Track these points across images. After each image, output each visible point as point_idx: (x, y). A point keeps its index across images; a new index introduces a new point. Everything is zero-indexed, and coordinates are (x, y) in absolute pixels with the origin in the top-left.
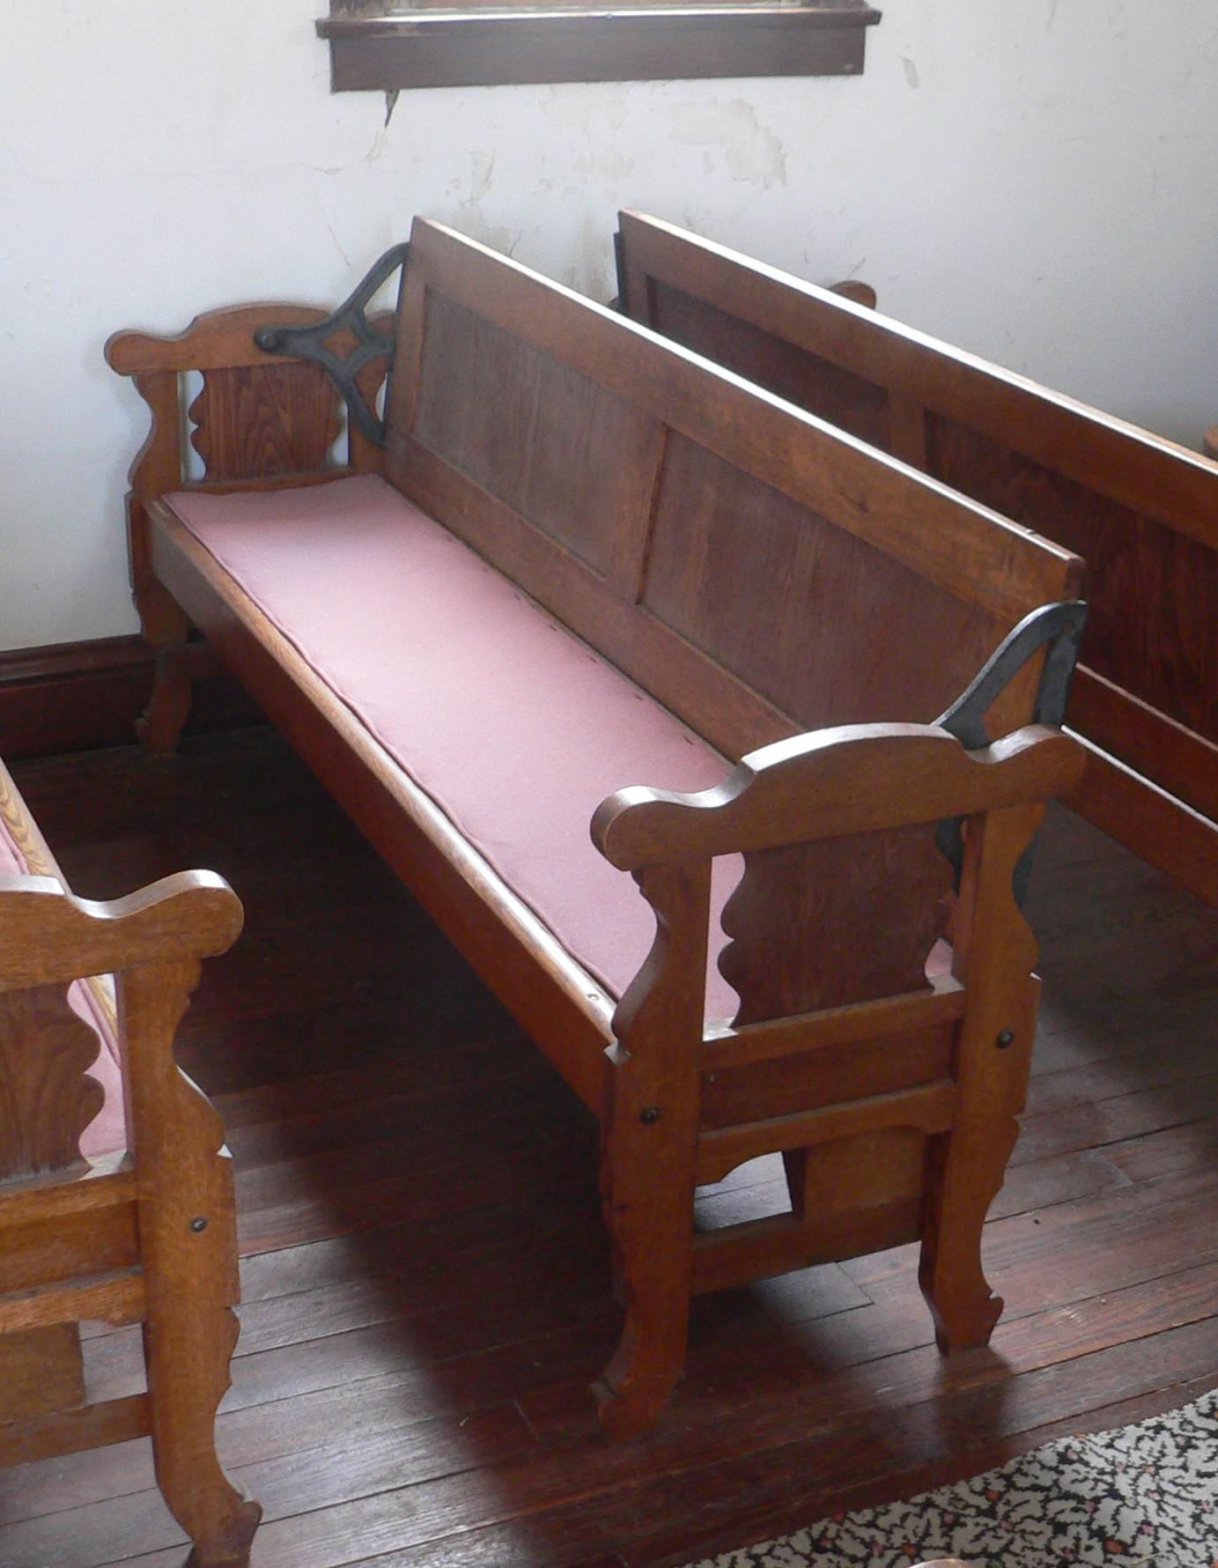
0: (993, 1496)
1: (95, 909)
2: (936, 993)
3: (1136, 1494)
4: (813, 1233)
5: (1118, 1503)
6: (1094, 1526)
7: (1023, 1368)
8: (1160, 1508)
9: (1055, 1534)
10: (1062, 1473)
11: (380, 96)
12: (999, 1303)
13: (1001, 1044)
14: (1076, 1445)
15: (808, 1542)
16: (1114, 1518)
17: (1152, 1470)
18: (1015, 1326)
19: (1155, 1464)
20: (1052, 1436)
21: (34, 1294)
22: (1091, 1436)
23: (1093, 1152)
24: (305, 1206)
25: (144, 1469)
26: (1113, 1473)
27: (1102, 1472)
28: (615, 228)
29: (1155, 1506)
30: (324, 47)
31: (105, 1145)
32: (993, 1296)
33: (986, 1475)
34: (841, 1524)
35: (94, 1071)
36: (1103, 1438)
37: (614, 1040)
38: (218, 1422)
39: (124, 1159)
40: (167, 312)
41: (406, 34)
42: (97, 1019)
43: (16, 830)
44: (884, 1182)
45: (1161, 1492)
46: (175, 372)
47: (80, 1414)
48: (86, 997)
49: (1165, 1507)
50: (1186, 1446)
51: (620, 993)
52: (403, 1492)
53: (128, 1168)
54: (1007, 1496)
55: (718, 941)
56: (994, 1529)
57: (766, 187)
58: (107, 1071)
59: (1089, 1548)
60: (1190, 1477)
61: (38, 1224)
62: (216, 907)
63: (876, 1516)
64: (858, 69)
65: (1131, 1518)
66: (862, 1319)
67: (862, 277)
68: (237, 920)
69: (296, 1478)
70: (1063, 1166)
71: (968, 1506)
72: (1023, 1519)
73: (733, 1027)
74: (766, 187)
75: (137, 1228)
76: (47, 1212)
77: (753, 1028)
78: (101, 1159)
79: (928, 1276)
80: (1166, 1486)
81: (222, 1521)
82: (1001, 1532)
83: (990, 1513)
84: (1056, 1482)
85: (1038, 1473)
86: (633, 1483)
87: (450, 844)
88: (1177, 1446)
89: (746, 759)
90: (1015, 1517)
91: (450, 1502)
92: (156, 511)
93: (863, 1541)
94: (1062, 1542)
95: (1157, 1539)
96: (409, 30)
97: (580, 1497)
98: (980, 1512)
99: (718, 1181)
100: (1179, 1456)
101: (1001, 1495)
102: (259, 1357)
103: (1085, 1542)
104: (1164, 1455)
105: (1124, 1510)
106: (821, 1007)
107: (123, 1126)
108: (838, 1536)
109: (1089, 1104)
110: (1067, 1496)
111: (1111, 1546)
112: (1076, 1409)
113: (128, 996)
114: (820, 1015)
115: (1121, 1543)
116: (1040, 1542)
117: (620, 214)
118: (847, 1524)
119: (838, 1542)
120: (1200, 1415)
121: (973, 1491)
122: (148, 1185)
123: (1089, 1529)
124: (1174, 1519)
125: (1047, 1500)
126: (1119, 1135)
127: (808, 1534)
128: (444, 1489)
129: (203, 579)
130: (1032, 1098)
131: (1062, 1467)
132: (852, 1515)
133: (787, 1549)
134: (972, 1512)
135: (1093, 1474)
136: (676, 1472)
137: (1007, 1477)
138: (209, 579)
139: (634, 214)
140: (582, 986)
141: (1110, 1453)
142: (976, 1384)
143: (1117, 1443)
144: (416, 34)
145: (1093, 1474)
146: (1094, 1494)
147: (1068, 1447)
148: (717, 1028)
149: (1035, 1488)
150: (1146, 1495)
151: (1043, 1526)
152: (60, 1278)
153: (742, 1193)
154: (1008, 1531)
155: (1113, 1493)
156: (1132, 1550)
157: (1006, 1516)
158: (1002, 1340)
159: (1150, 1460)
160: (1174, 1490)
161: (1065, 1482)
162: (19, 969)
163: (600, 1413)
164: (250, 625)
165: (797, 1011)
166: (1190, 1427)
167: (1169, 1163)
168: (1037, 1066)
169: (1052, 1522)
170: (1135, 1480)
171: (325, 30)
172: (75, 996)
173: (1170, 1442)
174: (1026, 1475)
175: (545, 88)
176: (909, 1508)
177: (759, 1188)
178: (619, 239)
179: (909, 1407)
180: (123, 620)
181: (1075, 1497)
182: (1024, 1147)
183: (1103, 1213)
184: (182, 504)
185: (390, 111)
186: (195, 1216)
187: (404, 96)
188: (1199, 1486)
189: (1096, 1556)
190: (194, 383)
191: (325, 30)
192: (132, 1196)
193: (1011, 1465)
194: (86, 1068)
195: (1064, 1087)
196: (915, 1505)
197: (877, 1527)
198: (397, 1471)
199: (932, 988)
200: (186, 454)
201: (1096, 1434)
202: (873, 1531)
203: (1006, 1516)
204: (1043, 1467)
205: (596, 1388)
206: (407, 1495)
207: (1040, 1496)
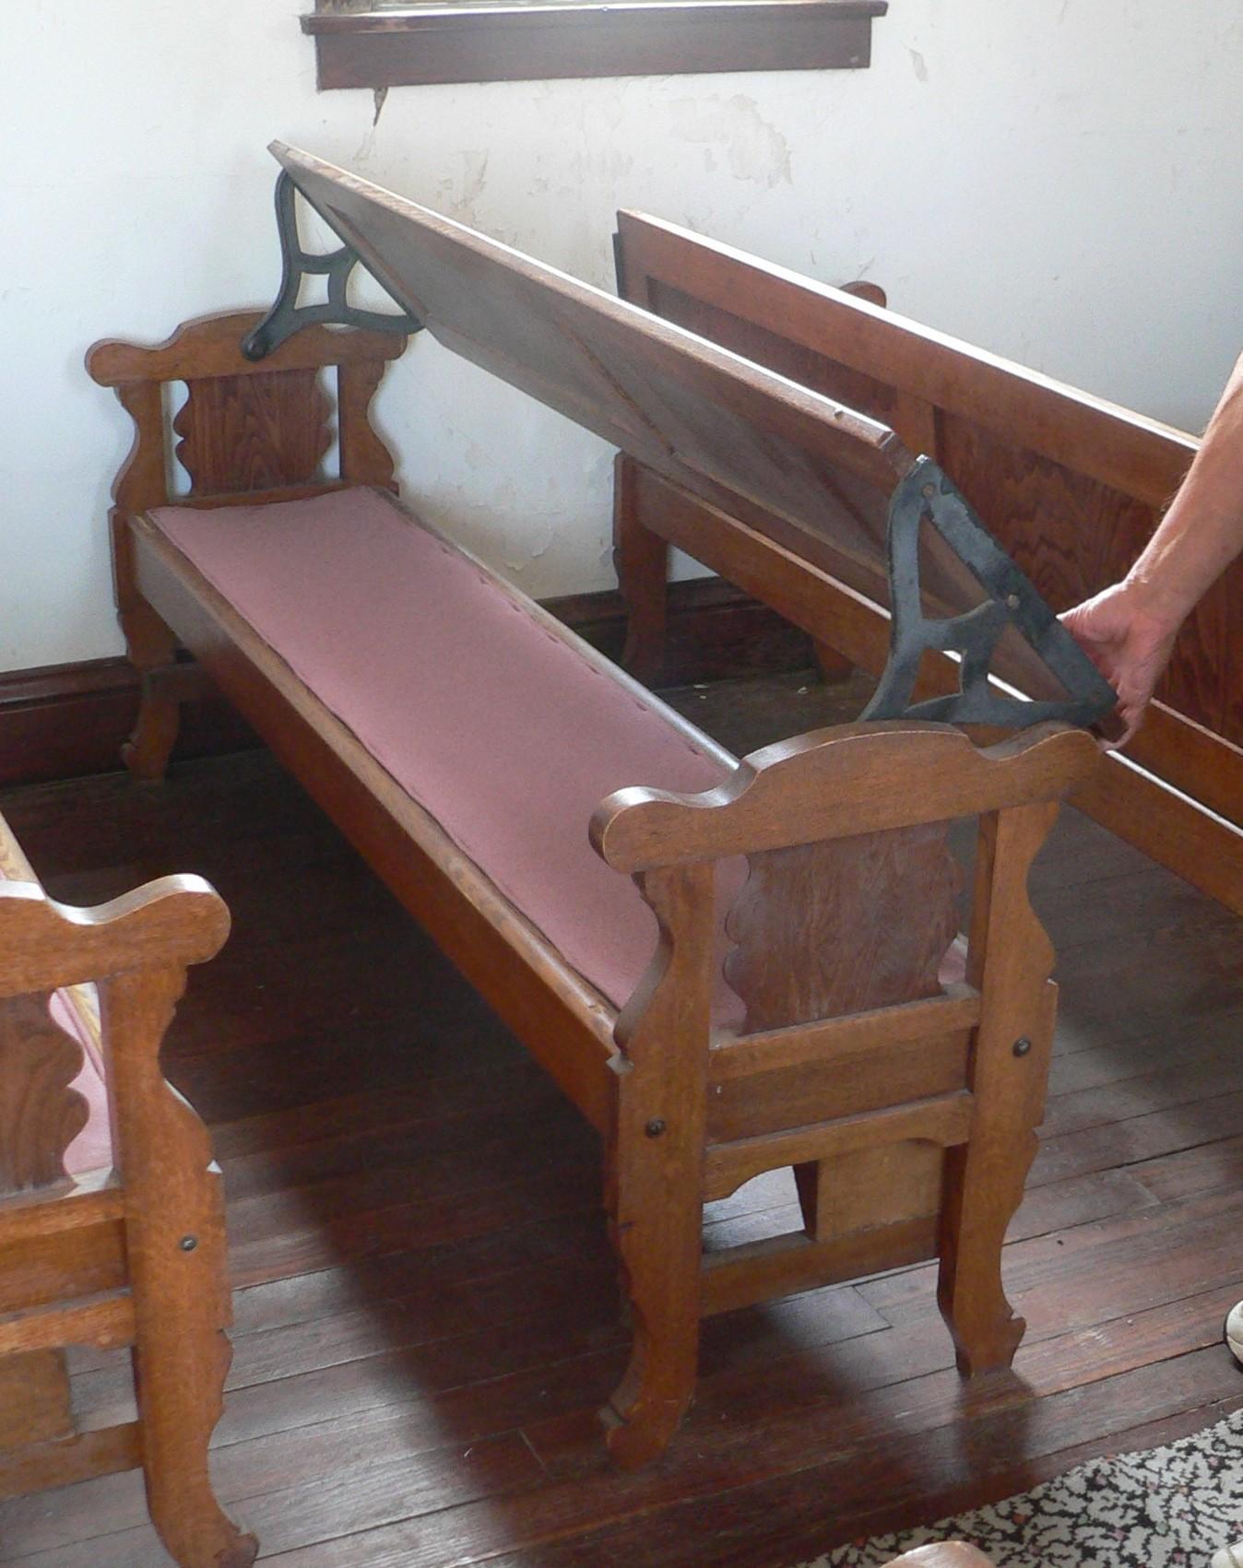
0: (1021, 1520)
1: (76, 915)
3: (1168, 1517)
4: (813, 1257)
5: (1149, 1531)
6: (1125, 1553)
8: (1194, 1530)
9: (1084, 1558)
10: (1090, 1500)
11: (367, 95)
12: (1021, 1324)
13: (1017, 1052)
14: (1106, 1468)
17: (1185, 1490)
18: (1038, 1348)
20: (1078, 1459)
21: (17, 1318)
22: (1122, 1456)
24: (300, 1236)
25: (137, 1505)
26: (1144, 1496)
27: (1132, 1496)
29: (1188, 1527)
30: (308, 45)
31: (89, 1162)
33: (1012, 1499)
34: (862, 1548)
35: (77, 1084)
36: (1134, 1458)
37: (616, 1051)
38: (211, 1457)
39: (111, 1175)
40: (152, 324)
41: (395, 30)
42: (76, 1026)
44: (905, 1196)
45: (1195, 1512)
46: (158, 383)
47: (69, 1444)
48: (68, 1010)
49: (1199, 1528)
50: (1220, 1467)
52: (405, 1525)
54: (1034, 1520)
56: (1020, 1553)
58: (91, 1084)
60: (1224, 1499)
61: (24, 1244)
62: (202, 912)
63: (898, 1541)
64: (865, 63)
65: (1162, 1547)
68: (223, 926)
69: (294, 1512)
71: (993, 1530)
72: (1051, 1543)
76: (30, 1231)
80: (1199, 1506)
82: (1028, 1557)
83: (1017, 1537)
84: (1085, 1510)
85: (1067, 1499)
88: (1210, 1467)
90: (1043, 1541)
91: (455, 1533)
92: (140, 525)
96: (397, 25)
97: (588, 1527)
98: (1006, 1536)
100: (1212, 1477)
101: (1028, 1519)
102: (255, 1390)
104: (1196, 1477)
105: (1154, 1539)
106: (833, 1013)
107: (108, 1144)
109: (1111, 1123)
110: (1097, 1524)
112: (1101, 1431)
113: (111, 1007)
114: (829, 1025)
117: (619, 214)
118: (869, 1549)
120: (1233, 1432)
121: (998, 1515)
122: (134, 1202)
124: (1208, 1540)
125: (1075, 1526)
127: (829, 1559)
128: (448, 1521)
131: (1090, 1494)
132: (874, 1540)
134: (998, 1536)
135: (1123, 1500)
136: (688, 1500)
139: (633, 214)
140: (582, 1001)
141: (1140, 1474)
143: (1148, 1464)
144: (405, 29)
145: (1123, 1500)
146: (1122, 1523)
147: (1097, 1471)
149: (1063, 1514)
150: (1179, 1516)
151: (1072, 1550)
152: (47, 1300)
153: (755, 1218)
154: (1035, 1555)
155: (1144, 1520)
157: (1034, 1540)
158: (1029, 1363)
159: (1183, 1481)
160: (1209, 1511)
161: (1094, 1510)
165: (806, 1018)
166: (1222, 1447)
167: (1196, 1177)
168: (1055, 1084)
169: (1080, 1546)
170: (1168, 1501)
171: (311, 26)
172: (57, 1007)
173: (1203, 1464)
174: (1054, 1501)
178: (618, 240)
179: (931, 1431)
180: (108, 642)
181: (1103, 1524)
182: (1041, 1168)
184: (168, 520)
187: (395, 95)
188: (1234, 1507)
190: (178, 394)
191: (311, 26)
192: (118, 1214)
193: (1038, 1491)
195: (1087, 1106)
198: (399, 1504)
201: (1127, 1454)
203: (1034, 1540)
204: (1072, 1494)
205: (605, 1415)
206: (409, 1527)
207: (1070, 1522)
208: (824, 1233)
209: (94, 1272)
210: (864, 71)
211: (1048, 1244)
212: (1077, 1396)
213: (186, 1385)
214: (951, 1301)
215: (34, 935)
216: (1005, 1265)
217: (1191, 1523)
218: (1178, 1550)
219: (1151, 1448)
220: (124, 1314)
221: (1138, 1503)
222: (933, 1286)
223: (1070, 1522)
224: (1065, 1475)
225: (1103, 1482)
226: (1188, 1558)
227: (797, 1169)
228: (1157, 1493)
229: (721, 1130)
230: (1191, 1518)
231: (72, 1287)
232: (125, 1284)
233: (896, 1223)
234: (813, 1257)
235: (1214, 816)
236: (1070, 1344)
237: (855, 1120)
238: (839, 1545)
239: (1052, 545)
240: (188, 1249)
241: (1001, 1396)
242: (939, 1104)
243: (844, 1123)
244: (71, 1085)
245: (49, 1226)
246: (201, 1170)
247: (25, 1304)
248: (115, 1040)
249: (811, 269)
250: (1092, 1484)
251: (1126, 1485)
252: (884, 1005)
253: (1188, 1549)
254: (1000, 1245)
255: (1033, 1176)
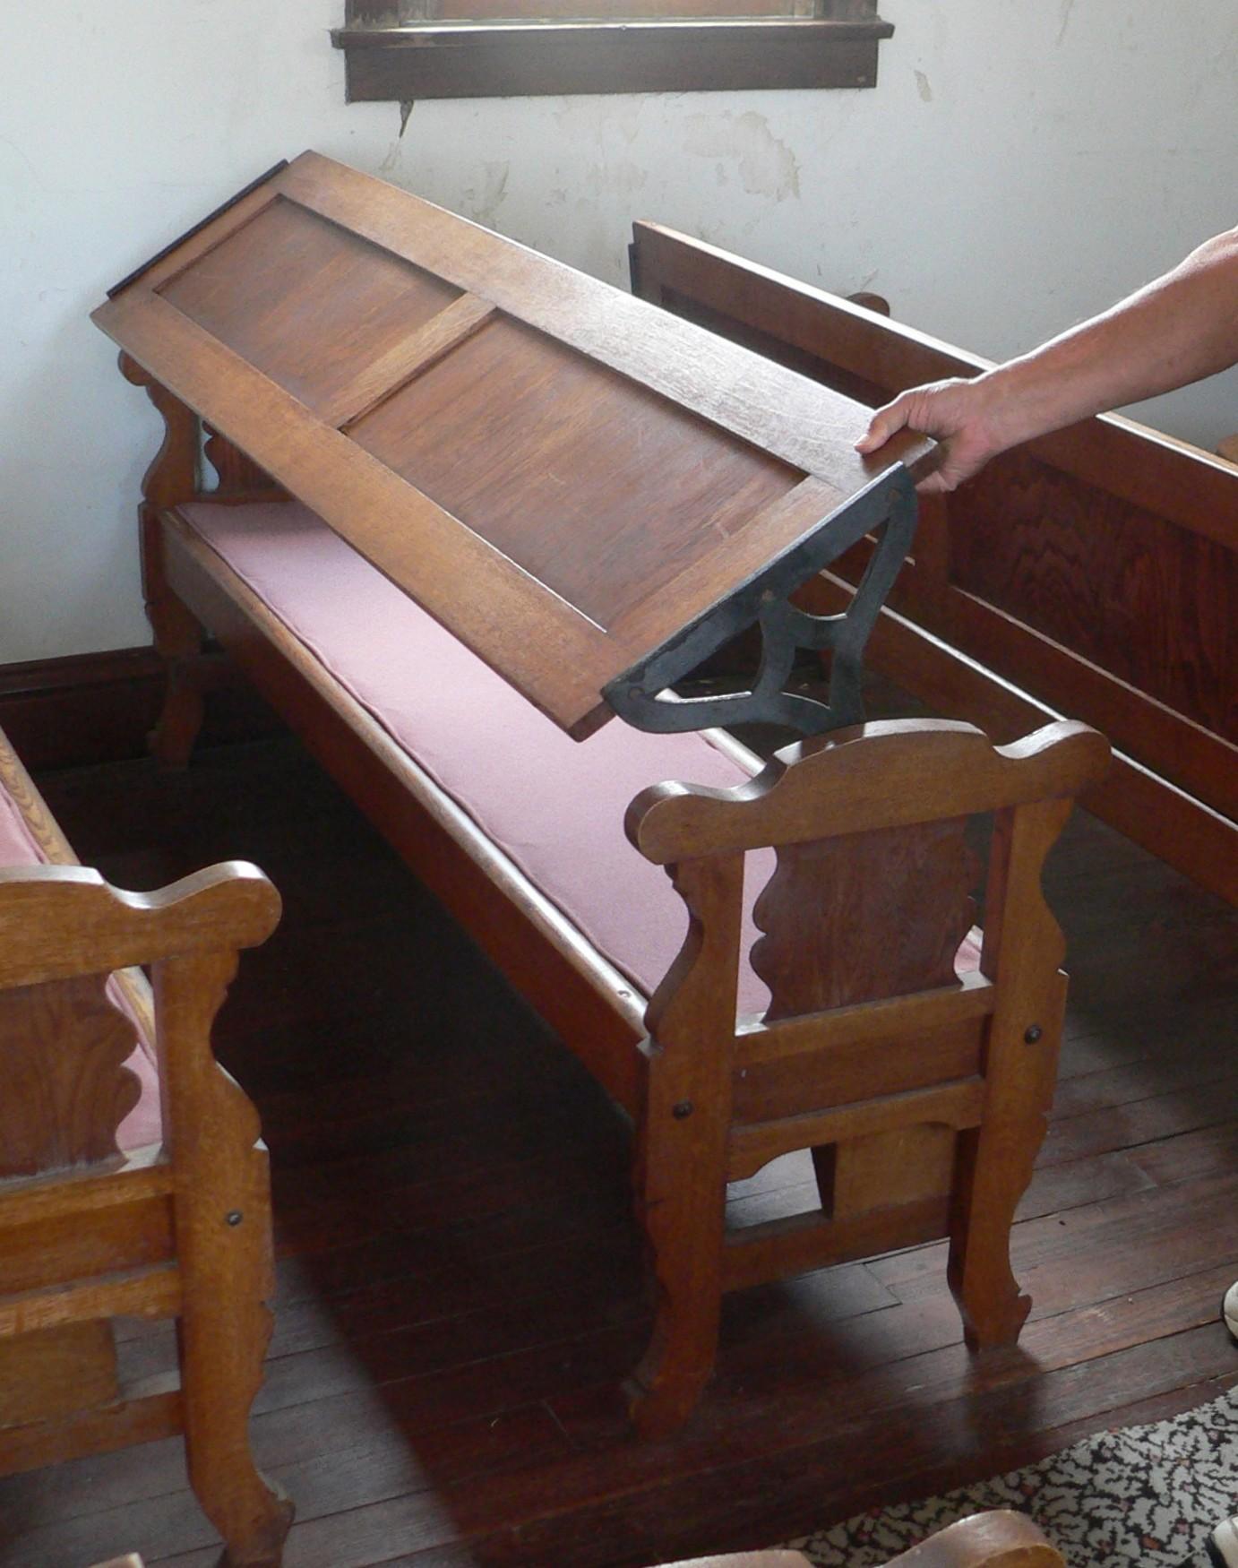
1: (134, 900)
2: (965, 988)
3: (1171, 1488)
4: (835, 1233)
5: (1153, 1502)
6: (1130, 1523)
7: (1051, 1366)
8: (1196, 1501)
11: (394, 108)
13: (1028, 1039)
14: (1110, 1441)
18: (1043, 1325)
19: (1189, 1458)
22: (1126, 1430)
23: (1116, 1155)
26: (1148, 1468)
27: (1136, 1468)
28: (630, 239)
30: (339, 57)
31: (140, 1140)
33: (1023, 1471)
34: (877, 1518)
35: (129, 1064)
36: (1137, 1432)
37: (647, 1035)
43: (40, 833)
44: (916, 1176)
45: (1197, 1484)
51: (652, 991)
53: (164, 1161)
55: (750, 934)
57: (779, 199)
58: (143, 1064)
59: (1125, 1542)
62: (254, 897)
63: (912, 1510)
64: (871, 82)
65: (1165, 1518)
66: (891, 1320)
68: (274, 913)
73: (764, 1022)
74: (779, 199)
76: (84, 1204)
77: (785, 1025)
78: (137, 1152)
79: (956, 1276)
80: (1201, 1479)
81: (255, 1521)
84: (1091, 1481)
87: (476, 846)
88: (1210, 1441)
89: (778, 753)
90: (1051, 1511)
92: (170, 521)
93: (899, 1534)
95: (1192, 1537)
99: (751, 1176)
100: (1213, 1450)
101: (1036, 1490)
103: (1121, 1535)
105: (1158, 1510)
106: (855, 1000)
108: (875, 1530)
110: (1103, 1495)
111: (1147, 1542)
112: (1105, 1406)
115: (1158, 1541)
116: (1076, 1536)
117: (635, 226)
118: (883, 1519)
119: (875, 1536)
123: (1124, 1525)
124: (1210, 1511)
125: (1081, 1497)
126: (1143, 1138)
127: (845, 1528)
129: (219, 588)
132: (889, 1509)
133: (824, 1544)
135: (1127, 1472)
136: (708, 1470)
138: (227, 589)
139: (649, 225)
141: (1144, 1447)
143: (1151, 1437)
144: (431, 44)
145: (1127, 1472)
146: (1127, 1494)
147: (1102, 1444)
148: (748, 1025)
149: (1071, 1485)
150: (1182, 1488)
152: (98, 1272)
155: (1148, 1492)
156: (1168, 1548)
157: (1042, 1510)
158: (1033, 1338)
159: (1185, 1455)
160: (1210, 1483)
161: (1099, 1481)
162: (58, 960)
163: (632, 1411)
164: (269, 634)
166: (1222, 1421)
167: (1195, 1164)
170: (1170, 1473)
173: (1203, 1438)
174: (1061, 1473)
175: (559, 99)
176: (945, 1503)
178: (634, 251)
180: (135, 631)
181: (1109, 1496)
182: (1050, 1148)
184: (197, 515)
185: (404, 123)
186: (230, 1210)
187: (420, 107)
189: (1133, 1549)
191: (341, 40)
192: (168, 1188)
193: (1046, 1463)
194: (125, 1057)
196: (951, 1500)
197: (913, 1521)
199: (961, 983)
200: (199, 464)
202: (909, 1525)
203: (1042, 1510)
204: (1078, 1466)
205: (627, 1386)
207: (1076, 1493)
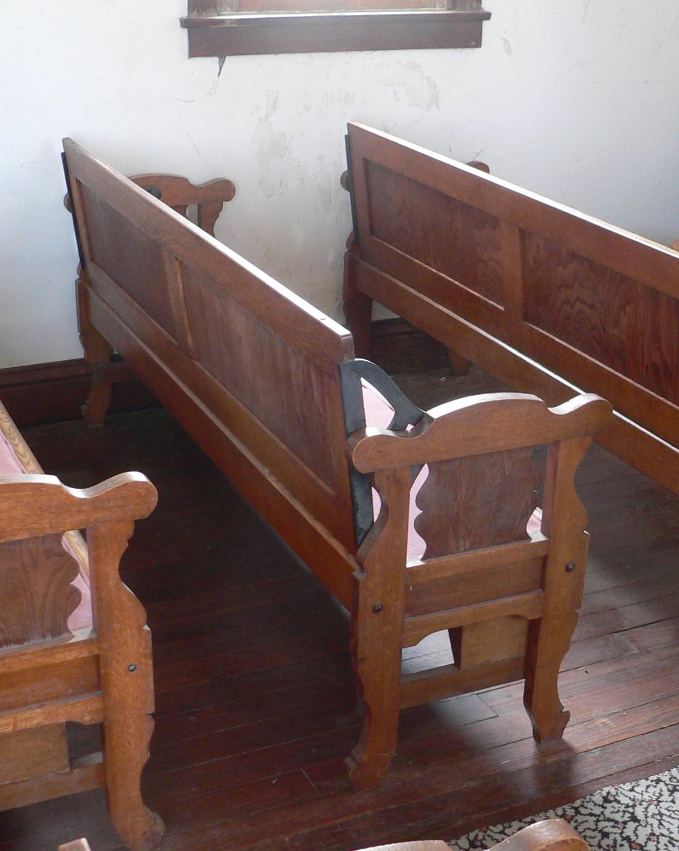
1: (78, 493)
2: (533, 541)
3: (646, 817)
4: (461, 677)
6: (624, 835)
7: (581, 750)
8: (661, 824)
10: (605, 808)
11: (215, 60)
13: (568, 570)
14: (613, 791)
15: (467, 842)
16: (634, 832)
17: (656, 803)
18: (576, 727)
21: (42, 706)
22: (622, 785)
26: (634, 806)
27: (627, 806)
30: (184, 34)
31: (81, 624)
32: (564, 710)
34: (486, 832)
36: (628, 786)
39: (92, 632)
44: (506, 647)
45: (661, 814)
53: (94, 636)
55: (414, 512)
57: (428, 110)
58: (82, 584)
59: (621, 845)
61: (47, 667)
62: (142, 492)
63: (504, 828)
64: (478, 44)
65: (643, 833)
66: (493, 725)
67: (480, 159)
70: (601, 643)
73: (422, 560)
74: (428, 110)
75: (98, 669)
77: (434, 561)
79: (528, 700)
80: (663, 811)
81: (144, 834)
84: (602, 813)
85: (593, 807)
86: (369, 813)
88: (669, 790)
90: (581, 829)
94: (606, 842)
95: (658, 842)
96: (232, 23)
97: (340, 820)
100: (670, 795)
101: (573, 817)
104: (662, 795)
105: (639, 828)
107: (91, 615)
108: (484, 839)
110: (609, 820)
111: (633, 845)
112: (611, 771)
114: (469, 554)
115: (639, 845)
116: (595, 842)
117: (349, 125)
118: (489, 832)
119: (484, 842)
122: (105, 646)
124: (668, 829)
125: (598, 821)
127: (468, 838)
130: (585, 607)
132: (491, 827)
135: (623, 808)
136: (392, 807)
137: (576, 809)
139: (356, 124)
141: (632, 794)
142: (555, 759)
143: (636, 789)
144: (235, 25)
145: (623, 808)
147: (608, 793)
148: (414, 560)
149: (591, 815)
150: (652, 817)
152: (57, 698)
153: (425, 658)
155: (634, 819)
158: (571, 735)
160: (668, 813)
161: (607, 813)
163: (350, 775)
165: (458, 550)
167: (660, 638)
169: (601, 831)
170: (646, 808)
171: (185, 23)
173: (665, 789)
177: (433, 655)
178: (348, 139)
179: (520, 771)
180: (70, 348)
181: (613, 820)
182: (579, 632)
183: (623, 667)
187: (229, 60)
192: (96, 652)
193: (578, 803)
195: (600, 600)
199: (530, 539)
204: (595, 804)
205: (348, 761)
207: (594, 819)
208: (465, 665)
209: (82, 682)
210: (477, 49)
211: (581, 673)
212: (597, 753)
213: (129, 743)
214: (531, 702)
215: (54, 504)
216: (559, 683)
217: (659, 820)
218: (653, 834)
219: (637, 780)
220: (98, 705)
221: (631, 810)
222: (521, 694)
223: (594, 819)
224: (591, 795)
225: (612, 799)
226: (658, 838)
227: (450, 631)
228: (641, 804)
229: (410, 610)
230: (659, 817)
231: (70, 691)
232: (99, 689)
233: (503, 660)
234: (461, 677)
235: (670, 446)
236: (593, 725)
237: (483, 605)
238: (473, 830)
239: (582, 302)
240: (133, 671)
241: (557, 752)
242: (526, 597)
243: (477, 606)
244: (72, 583)
245: (59, 658)
246: (140, 629)
247: (46, 700)
248: (95, 560)
249: (449, 153)
250: (606, 800)
251: (624, 800)
252: (498, 544)
253: (657, 834)
254: (557, 672)
255: (574, 638)
